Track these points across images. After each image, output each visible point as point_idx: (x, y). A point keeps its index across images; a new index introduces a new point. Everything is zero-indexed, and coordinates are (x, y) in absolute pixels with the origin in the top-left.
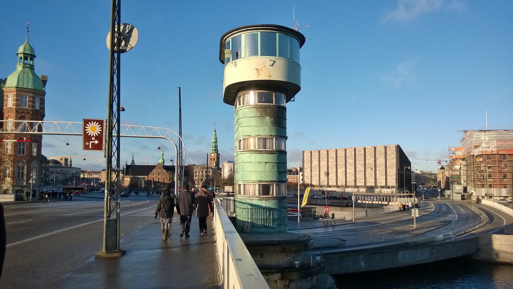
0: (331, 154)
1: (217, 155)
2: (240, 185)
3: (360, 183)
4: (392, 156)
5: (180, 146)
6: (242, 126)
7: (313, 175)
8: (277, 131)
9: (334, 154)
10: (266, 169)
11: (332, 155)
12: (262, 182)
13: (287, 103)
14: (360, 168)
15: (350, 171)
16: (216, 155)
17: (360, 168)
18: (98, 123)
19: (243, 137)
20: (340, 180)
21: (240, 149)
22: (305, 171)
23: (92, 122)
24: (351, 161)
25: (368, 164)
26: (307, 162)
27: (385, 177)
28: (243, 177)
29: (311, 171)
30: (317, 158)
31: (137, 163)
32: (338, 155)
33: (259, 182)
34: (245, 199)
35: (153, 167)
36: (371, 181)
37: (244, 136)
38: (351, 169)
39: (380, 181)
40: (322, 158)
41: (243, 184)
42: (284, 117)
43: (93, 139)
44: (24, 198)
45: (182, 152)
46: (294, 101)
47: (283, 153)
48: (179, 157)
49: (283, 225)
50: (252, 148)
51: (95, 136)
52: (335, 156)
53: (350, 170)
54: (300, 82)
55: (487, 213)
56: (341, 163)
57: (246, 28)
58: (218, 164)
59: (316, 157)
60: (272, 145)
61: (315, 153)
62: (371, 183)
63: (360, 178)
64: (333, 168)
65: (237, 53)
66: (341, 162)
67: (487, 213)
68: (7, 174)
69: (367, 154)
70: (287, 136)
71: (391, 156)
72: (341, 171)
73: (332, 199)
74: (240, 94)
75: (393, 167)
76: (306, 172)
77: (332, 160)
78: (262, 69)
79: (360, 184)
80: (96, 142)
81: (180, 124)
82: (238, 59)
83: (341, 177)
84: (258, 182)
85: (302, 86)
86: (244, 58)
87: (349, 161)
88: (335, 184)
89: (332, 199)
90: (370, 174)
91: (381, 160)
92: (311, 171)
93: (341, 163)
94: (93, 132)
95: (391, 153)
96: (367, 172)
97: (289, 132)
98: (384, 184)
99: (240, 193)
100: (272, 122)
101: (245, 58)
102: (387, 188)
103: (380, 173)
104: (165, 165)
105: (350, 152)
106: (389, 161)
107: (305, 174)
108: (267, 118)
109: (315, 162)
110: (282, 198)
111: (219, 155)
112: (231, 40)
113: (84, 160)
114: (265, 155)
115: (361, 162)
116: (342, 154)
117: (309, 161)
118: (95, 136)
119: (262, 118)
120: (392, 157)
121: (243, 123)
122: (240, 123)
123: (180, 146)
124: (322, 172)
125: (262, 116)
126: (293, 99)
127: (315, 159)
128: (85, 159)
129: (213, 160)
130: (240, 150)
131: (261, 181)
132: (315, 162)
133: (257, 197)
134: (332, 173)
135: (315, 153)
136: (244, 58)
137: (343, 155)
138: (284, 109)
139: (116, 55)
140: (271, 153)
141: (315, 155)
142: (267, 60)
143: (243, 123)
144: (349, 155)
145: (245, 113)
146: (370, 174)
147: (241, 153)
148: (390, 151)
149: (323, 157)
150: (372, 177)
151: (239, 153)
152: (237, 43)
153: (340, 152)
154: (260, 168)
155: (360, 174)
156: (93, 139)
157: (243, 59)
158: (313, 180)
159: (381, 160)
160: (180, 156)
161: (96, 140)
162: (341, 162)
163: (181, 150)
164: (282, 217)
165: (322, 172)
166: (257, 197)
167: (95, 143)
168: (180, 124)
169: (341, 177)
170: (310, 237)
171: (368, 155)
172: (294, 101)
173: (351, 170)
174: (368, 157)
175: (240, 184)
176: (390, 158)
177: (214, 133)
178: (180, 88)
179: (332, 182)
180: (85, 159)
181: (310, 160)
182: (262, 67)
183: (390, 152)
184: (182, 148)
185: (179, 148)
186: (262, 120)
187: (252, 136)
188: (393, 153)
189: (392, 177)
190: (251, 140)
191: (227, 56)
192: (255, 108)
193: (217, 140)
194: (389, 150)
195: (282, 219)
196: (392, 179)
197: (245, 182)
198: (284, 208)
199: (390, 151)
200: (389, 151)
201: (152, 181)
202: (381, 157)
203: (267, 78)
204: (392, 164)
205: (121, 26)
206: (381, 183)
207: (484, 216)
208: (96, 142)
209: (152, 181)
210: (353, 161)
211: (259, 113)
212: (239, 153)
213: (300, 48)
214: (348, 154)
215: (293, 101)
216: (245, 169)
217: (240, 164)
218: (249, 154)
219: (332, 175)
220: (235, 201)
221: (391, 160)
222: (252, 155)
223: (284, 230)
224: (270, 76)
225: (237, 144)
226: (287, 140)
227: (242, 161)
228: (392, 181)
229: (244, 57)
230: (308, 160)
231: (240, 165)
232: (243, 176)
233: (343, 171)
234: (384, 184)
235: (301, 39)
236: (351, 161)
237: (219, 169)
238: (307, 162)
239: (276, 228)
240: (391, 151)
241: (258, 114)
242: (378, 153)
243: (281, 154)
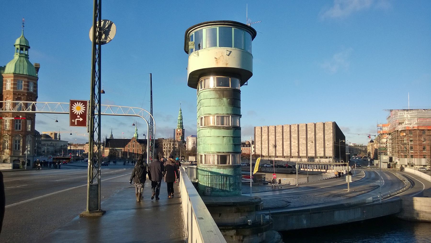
0: (278, 129)
1: (182, 130)
2: (201, 156)
3: (302, 154)
4: (329, 131)
5: (152, 123)
6: (203, 106)
7: (263, 147)
8: (233, 110)
9: (280, 129)
10: (223, 142)
11: (279, 130)
12: (220, 153)
13: (241, 86)
14: (303, 141)
15: (294, 144)
16: (181, 130)
17: (303, 141)
18: (82, 104)
19: (204, 115)
20: (286, 151)
21: (202, 125)
22: (257, 144)
23: (77, 102)
24: (295, 135)
25: (309, 138)
26: (258, 136)
27: (323, 149)
28: (204, 148)
29: (261, 143)
30: (266, 133)
31: (115, 137)
32: (284, 130)
33: (218, 153)
34: (205, 167)
35: (129, 141)
36: (312, 152)
37: (205, 115)
38: (295, 142)
39: (319, 152)
40: (271, 133)
41: (204, 155)
42: (238, 99)
43: (78, 117)
44: (20, 167)
45: (153, 128)
46: (247, 85)
47: (238, 129)
48: (150, 132)
49: (238, 189)
50: (212, 124)
51: (79, 114)
52: (281, 131)
53: (294, 143)
54: (252, 69)
55: (409, 179)
56: (286, 137)
57: (207, 24)
58: (183, 138)
59: (265, 132)
60: (229, 122)
61: (264, 129)
62: (311, 154)
63: (303, 149)
64: (280, 141)
65: (199, 45)
66: (287, 136)
67: (409, 179)
68: (6, 146)
69: (308, 129)
70: (241, 114)
71: (328, 131)
72: (286, 144)
73: (279, 167)
74: (202, 79)
75: (330, 140)
76: (257, 145)
77: (279, 135)
78: (220, 58)
79: (303, 154)
80: (81, 119)
81: (152, 104)
82: (200, 49)
83: (286, 149)
84: (217, 153)
85: (254, 72)
86: (205, 49)
87: (293, 136)
88: (281, 155)
89: (279, 167)
90: (311, 146)
91: (320, 135)
92: (261, 143)
93: (286, 137)
94: (78, 111)
95: (328, 129)
96: (308, 145)
97: (243, 111)
98: (322, 155)
99: (201, 162)
100: (229, 102)
101: (206, 49)
102: (325, 158)
103: (319, 145)
104: (139, 139)
105: (294, 128)
106: (327, 136)
107: (257, 147)
108: (225, 99)
109: (265, 137)
110: (237, 166)
111: (184, 131)
112: (194, 33)
113: (70, 134)
114: (223, 131)
115: (303, 137)
116: (287, 130)
117: (260, 135)
118: (79, 114)
119: (220, 99)
120: (329, 132)
121: (204, 103)
122: (202, 104)
123: (151, 123)
124: (271, 144)
125: (220, 98)
126: (246, 83)
127: (265, 134)
128: (71, 134)
129: (179, 134)
130: (202, 127)
131: (219, 153)
132: (265, 137)
133: (216, 166)
134: (279, 146)
135: (264, 129)
136: (205, 49)
137: (288, 131)
138: (239, 91)
139: (97, 46)
140: (228, 128)
141: (265, 130)
142: (224, 50)
143: (204, 103)
144: (293, 131)
145: (206, 95)
146: (311, 146)
147: (203, 129)
148: (328, 127)
149: (271, 132)
150: (312, 149)
151: (201, 129)
152: (199, 36)
153: (286, 127)
154: (219, 141)
155: (302, 146)
156: (78, 117)
157: (205, 49)
158: (263, 152)
159: (320, 135)
160: (151, 131)
161: (80, 118)
162: (287, 136)
163: (152, 127)
164: (237, 182)
165: (271, 144)
166: (216, 166)
167: (80, 120)
168: (152, 104)
169: (286, 149)
170: (261, 199)
171: (309, 130)
172: (247, 85)
173: (295, 143)
174: (309, 132)
175: (202, 154)
176: (328, 133)
177: (180, 112)
178: (151, 74)
179: (279, 153)
180: (71, 134)
181: (260, 134)
182: (220, 57)
183: (328, 127)
184: (153, 125)
185: (151, 124)
186: (220, 101)
187: (212, 114)
188: (330, 128)
189: (329, 149)
190: (211, 118)
191: (190, 47)
192: (215, 91)
193: (182, 118)
194: (326, 126)
195: (237, 184)
196: (330, 151)
197: (206, 153)
198: (238, 175)
199: (328, 127)
200: (327, 127)
201: (128, 152)
202: (320, 132)
203: (224, 66)
204: (329, 138)
205: (102, 22)
206: (320, 154)
207: (406, 182)
208: (81, 119)
209: (128, 152)
210: (296, 135)
211: (217, 95)
212: (201, 129)
213: (252, 40)
214: (292, 130)
215: (246, 85)
216: (206, 142)
217: (202, 138)
218: (210, 130)
219: (279, 147)
220: (197, 169)
221: (328, 134)
222: (212, 130)
223: (238, 193)
224: (227, 64)
225: (199, 121)
226: (241, 118)
227: (204, 135)
228: (330, 152)
229: (205, 48)
230: (259, 135)
231: (202, 139)
232: (204, 148)
233: (288, 143)
234: (323, 155)
235: (253, 33)
236: (295, 135)
237: (184, 142)
238: (258, 136)
239: (232, 192)
240: (329, 127)
241: (217, 96)
242: (318, 129)
243: (236, 130)
